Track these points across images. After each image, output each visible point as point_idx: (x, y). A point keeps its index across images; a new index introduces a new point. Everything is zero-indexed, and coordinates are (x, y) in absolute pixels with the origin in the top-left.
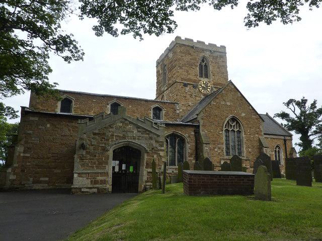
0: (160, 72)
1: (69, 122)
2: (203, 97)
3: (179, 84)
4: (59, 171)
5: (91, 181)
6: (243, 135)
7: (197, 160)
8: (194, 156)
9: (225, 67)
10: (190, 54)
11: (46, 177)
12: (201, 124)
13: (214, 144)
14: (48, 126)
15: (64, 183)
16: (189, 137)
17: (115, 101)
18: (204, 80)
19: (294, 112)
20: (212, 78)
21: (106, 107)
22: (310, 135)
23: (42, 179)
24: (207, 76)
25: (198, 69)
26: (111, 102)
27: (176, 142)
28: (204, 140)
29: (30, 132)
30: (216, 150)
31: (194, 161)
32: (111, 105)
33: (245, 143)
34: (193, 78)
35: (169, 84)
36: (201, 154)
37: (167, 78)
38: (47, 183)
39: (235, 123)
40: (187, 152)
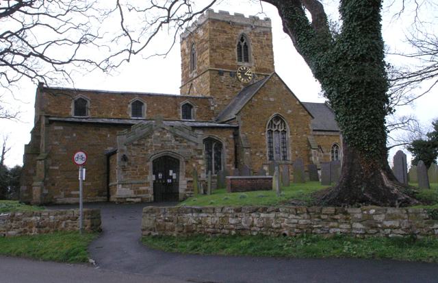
0: (187, 51)
1: (95, 130)
2: (242, 87)
4: (90, 184)
6: (288, 135)
7: (236, 167)
8: (232, 162)
9: (270, 46)
10: (225, 32)
12: (241, 125)
13: (256, 148)
14: (74, 135)
15: (95, 196)
17: (137, 98)
21: (127, 106)
24: (247, 60)
26: (131, 101)
27: (211, 147)
28: (244, 143)
30: (257, 154)
31: (233, 168)
32: (133, 104)
33: (291, 144)
34: (230, 63)
35: (200, 71)
36: (241, 160)
37: (196, 62)
39: (279, 122)
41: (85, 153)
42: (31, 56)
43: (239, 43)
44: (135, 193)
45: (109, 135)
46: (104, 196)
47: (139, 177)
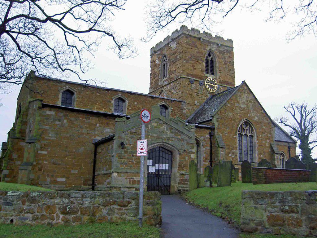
0: (157, 62)
3: (185, 79)
5: (130, 181)
6: (255, 139)
9: (232, 63)
10: (196, 47)
11: (64, 177)
12: (216, 126)
16: (204, 140)
18: (211, 78)
19: (294, 116)
20: (219, 74)
22: (311, 143)
23: (59, 179)
24: (212, 73)
25: (204, 64)
26: (116, 97)
29: (47, 127)
30: (230, 155)
34: (200, 74)
35: (171, 79)
38: (64, 184)
39: (247, 127)
40: (202, 157)
41: (149, 112)
42: (48, 21)
43: (207, 57)
44: (130, 183)
45: (98, 125)
46: (89, 185)
47: (134, 167)
